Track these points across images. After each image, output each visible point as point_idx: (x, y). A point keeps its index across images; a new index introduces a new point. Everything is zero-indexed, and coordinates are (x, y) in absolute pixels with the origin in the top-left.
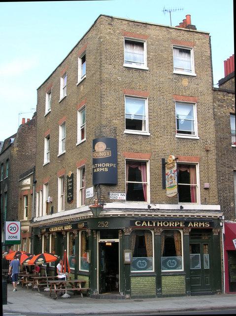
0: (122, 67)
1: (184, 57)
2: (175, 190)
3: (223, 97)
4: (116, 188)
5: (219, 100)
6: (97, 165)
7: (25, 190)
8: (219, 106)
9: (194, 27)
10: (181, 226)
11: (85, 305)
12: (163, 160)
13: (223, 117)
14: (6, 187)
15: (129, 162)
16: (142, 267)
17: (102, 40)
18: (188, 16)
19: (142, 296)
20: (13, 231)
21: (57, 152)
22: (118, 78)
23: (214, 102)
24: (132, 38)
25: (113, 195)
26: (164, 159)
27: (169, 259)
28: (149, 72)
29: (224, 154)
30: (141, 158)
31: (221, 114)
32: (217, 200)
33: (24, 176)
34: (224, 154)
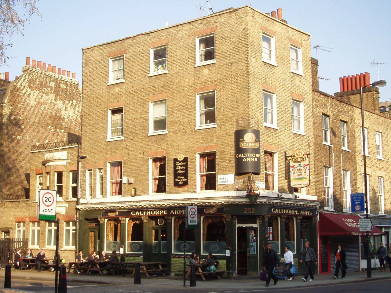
6: (247, 155)
10: (164, 213)
11: (204, 289)
20: (48, 203)
29: (318, 150)
31: (317, 113)
34: (318, 150)
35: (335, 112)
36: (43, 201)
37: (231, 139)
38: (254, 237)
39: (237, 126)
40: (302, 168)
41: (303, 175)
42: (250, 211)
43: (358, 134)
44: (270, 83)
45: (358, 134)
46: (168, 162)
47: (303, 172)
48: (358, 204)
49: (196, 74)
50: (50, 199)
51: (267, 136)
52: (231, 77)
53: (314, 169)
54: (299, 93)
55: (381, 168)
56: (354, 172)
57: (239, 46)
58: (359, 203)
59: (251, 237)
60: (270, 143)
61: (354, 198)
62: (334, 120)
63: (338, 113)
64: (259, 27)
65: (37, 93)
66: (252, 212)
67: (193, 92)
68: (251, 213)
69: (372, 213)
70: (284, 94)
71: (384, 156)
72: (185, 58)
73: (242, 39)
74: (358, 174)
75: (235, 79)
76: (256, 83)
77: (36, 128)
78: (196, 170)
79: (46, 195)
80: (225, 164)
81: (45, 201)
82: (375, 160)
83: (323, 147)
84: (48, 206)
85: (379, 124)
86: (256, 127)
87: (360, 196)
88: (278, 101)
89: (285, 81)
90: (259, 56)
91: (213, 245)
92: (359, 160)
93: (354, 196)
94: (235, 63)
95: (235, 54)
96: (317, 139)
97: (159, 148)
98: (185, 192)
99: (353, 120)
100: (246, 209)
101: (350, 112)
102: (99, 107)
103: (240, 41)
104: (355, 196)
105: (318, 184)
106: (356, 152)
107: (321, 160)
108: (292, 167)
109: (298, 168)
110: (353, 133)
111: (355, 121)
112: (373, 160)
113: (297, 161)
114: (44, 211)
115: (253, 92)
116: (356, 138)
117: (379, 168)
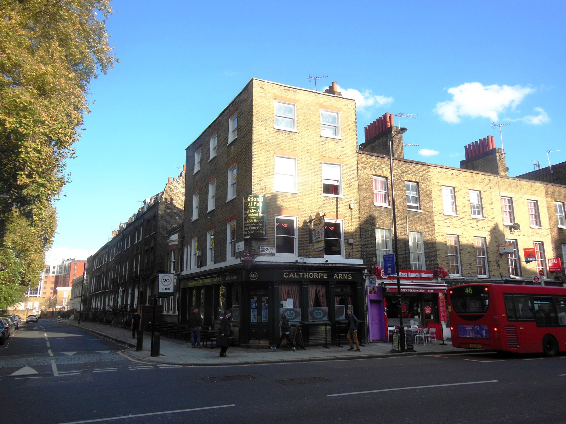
2: (323, 245)
3: (366, 159)
4: (266, 243)
5: (362, 163)
7: (173, 245)
8: (363, 167)
10: (324, 277)
13: (366, 178)
14: (153, 242)
15: (525, 250)
16: (318, 317)
20: (166, 283)
21: (207, 208)
25: (263, 249)
32: (360, 255)
33: (172, 232)
36: (161, 282)
44: (288, 149)
48: (390, 267)
61: (386, 259)
79: (166, 277)
83: (374, 209)
84: (168, 285)
87: (391, 257)
91: (316, 311)
96: (364, 201)
101: (422, 172)
106: (433, 212)
111: (431, 180)
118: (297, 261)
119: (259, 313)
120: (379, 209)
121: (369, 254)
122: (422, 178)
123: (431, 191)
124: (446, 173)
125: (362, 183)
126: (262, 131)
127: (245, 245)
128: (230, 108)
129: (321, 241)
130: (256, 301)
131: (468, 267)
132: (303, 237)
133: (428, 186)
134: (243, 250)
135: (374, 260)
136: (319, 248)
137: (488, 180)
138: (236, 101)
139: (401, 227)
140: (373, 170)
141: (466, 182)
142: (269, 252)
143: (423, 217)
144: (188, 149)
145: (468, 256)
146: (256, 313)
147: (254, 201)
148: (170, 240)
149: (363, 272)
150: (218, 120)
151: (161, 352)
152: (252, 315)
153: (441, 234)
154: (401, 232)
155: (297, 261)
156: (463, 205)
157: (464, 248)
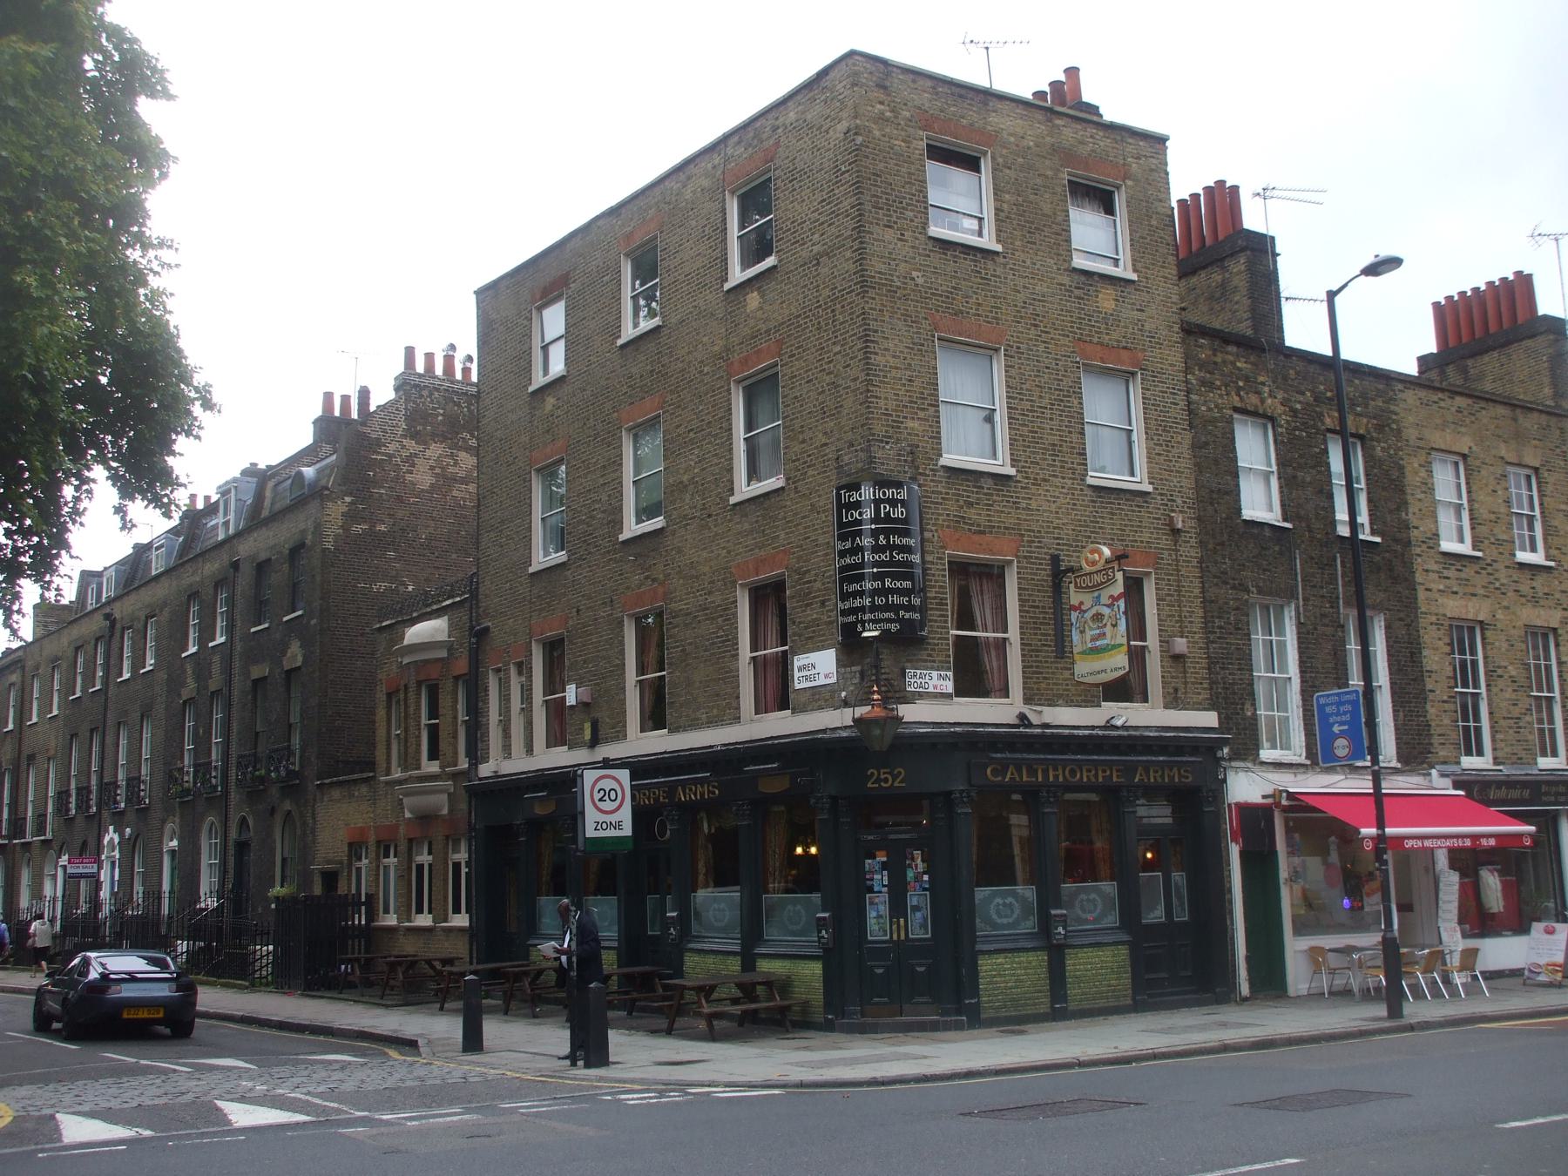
0: (922, 237)
1: (959, 177)
4: (924, 655)
8: (1203, 383)
9: (1094, 109)
10: (1115, 779)
12: (1055, 560)
16: (1005, 921)
17: (859, 139)
18: (1072, 72)
19: (1015, 1021)
20: (608, 805)
22: (915, 274)
23: (1187, 370)
24: (947, 140)
26: (1058, 556)
27: (1084, 889)
28: (1002, 260)
29: (1222, 544)
30: (992, 552)
31: (1210, 409)
32: (1205, 695)
34: (1222, 544)
35: (1300, 402)
37: (824, 522)
38: (924, 873)
39: (838, 473)
40: (1106, 611)
41: (1108, 635)
42: (886, 780)
43: (1418, 479)
45: (1418, 479)
46: (670, 623)
47: (1109, 624)
48: (1342, 734)
49: (731, 312)
50: (613, 793)
51: (961, 503)
52: (817, 307)
53: (1201, 614)
54: (1118, 341)
55: (1541, 595)
56: (1402, 615)
57: (834, 195)
58: (1346, 727)
59: (910, 874)
60: (979, 525)
61: (1328, 710)
62: (1297, 433)
63: (1317, 406)
64: (910, 121)
65: (436, 450)
66: (896, 784)
67: (722, 377)
68: (892, 785)
69: (1499, 764)
70: (1041, 348)
71: (1554, 552)
72: (703, 267)
73: (843, 169)
74: (1423, 622)
75: (829, 311)
76: (902, 315)
77: (436, 554)
78: (737, 644)
80: (813, 614)
81: (600, 800)
82: (1507, 567)
83: (1241, 530)
85: (1519, 437)
86: (905, 472)
87: (1349, 702)
88: (1013, 372)
89: (1044, 301)
90: (912, 221)
91: (999, 900)
92: (1427, 571)
93: (1328, 705)
94: (828, 254)
95: (826, 225)
96: (1212, 504)
97: (647, 578)
98: (711, 722)
99: (1392, 429)
100: (900, 773)
102: (513, 468)
103: (837, 177)
104: (1332, 704)
105: (1223, 668)
106: (1410, 542)
107: (1234, 579)
108: (1075, 608)
109: (1094, 611)
110: (1394, 474)
111: (1399, 431)
112: (1497, 571)
113: (1088, 587)
114: (599, 827)
115: (886, 349)
116: (1409, 491)
117: (1529, 598)
118: (1022, 717)
119: (898, 907)
120: (1256, 531)
121: (1235, 693)
122: (1375, 422)
123: (1401, 468)
124: (1442, 404)
125: (1203, 439)
126: (891, 246)
127: (840, 663)
128: (730, 151)
129: (1115, 647)
130: (884, 866)
131: (1511, 731)
132: (1036, 634)
133: (1392, 452)
134: (833, 680)
135: (1249, 714)
136: (1105, 671)
137: (1558, 431)
138: (758, 124)
139: (1323, 597)
140: (1233, 393)
141: (1499, 437)
142: (935, 687)
143: (1383, 558)
144: (489, 296)
145: (1508, 694)
146: (884, 909)
147: (883, 501)
148: (406, 642)
149: (1219, 754)
150: (657, 191)
151: (611, 1059)
152: (871, 914)
153: (1434, 619)
154: (1321, 615)
155: (1022, 717)
156: (1493, 517)
157: (1499, 667)
